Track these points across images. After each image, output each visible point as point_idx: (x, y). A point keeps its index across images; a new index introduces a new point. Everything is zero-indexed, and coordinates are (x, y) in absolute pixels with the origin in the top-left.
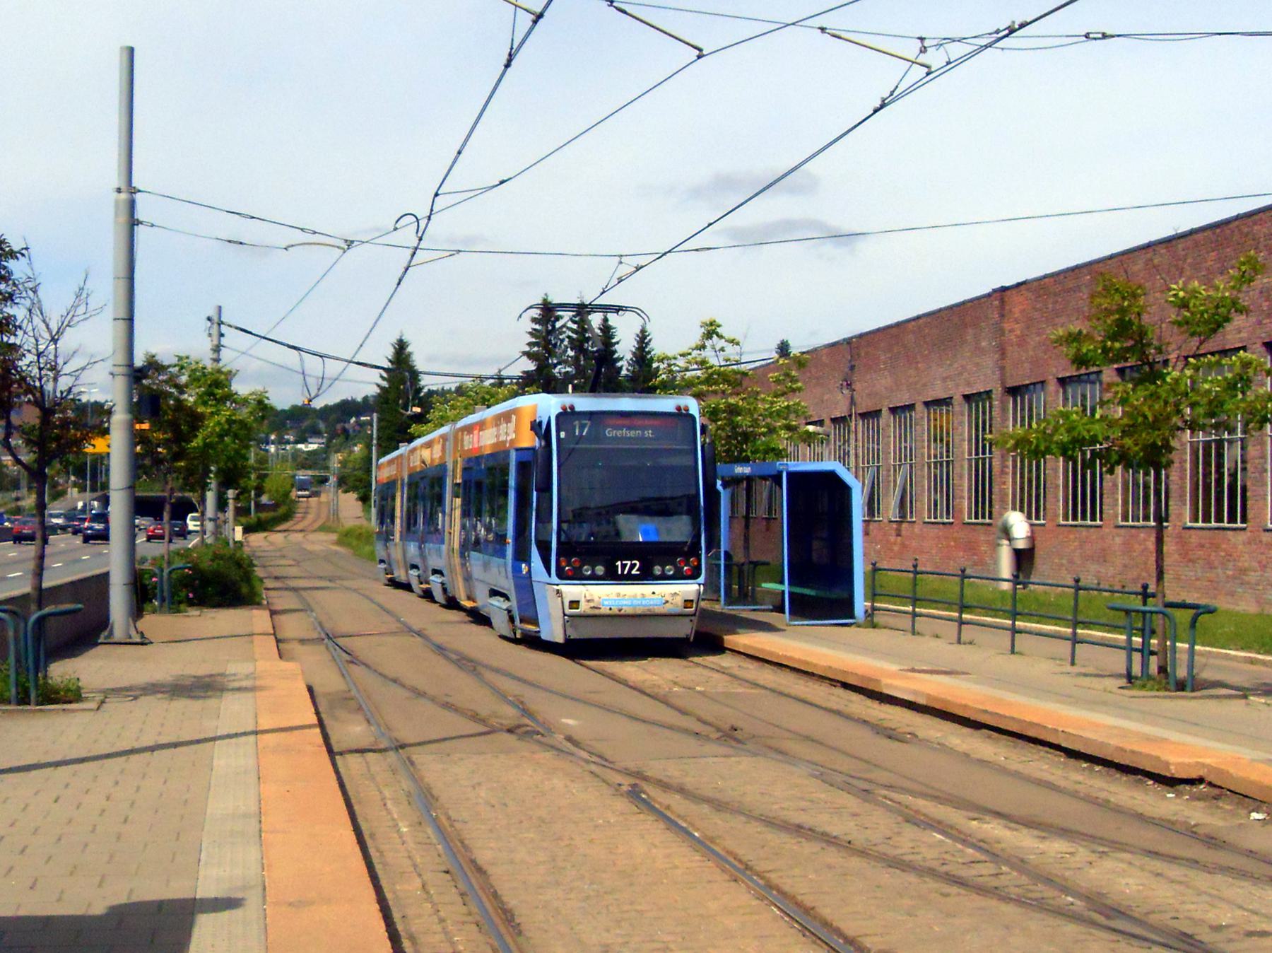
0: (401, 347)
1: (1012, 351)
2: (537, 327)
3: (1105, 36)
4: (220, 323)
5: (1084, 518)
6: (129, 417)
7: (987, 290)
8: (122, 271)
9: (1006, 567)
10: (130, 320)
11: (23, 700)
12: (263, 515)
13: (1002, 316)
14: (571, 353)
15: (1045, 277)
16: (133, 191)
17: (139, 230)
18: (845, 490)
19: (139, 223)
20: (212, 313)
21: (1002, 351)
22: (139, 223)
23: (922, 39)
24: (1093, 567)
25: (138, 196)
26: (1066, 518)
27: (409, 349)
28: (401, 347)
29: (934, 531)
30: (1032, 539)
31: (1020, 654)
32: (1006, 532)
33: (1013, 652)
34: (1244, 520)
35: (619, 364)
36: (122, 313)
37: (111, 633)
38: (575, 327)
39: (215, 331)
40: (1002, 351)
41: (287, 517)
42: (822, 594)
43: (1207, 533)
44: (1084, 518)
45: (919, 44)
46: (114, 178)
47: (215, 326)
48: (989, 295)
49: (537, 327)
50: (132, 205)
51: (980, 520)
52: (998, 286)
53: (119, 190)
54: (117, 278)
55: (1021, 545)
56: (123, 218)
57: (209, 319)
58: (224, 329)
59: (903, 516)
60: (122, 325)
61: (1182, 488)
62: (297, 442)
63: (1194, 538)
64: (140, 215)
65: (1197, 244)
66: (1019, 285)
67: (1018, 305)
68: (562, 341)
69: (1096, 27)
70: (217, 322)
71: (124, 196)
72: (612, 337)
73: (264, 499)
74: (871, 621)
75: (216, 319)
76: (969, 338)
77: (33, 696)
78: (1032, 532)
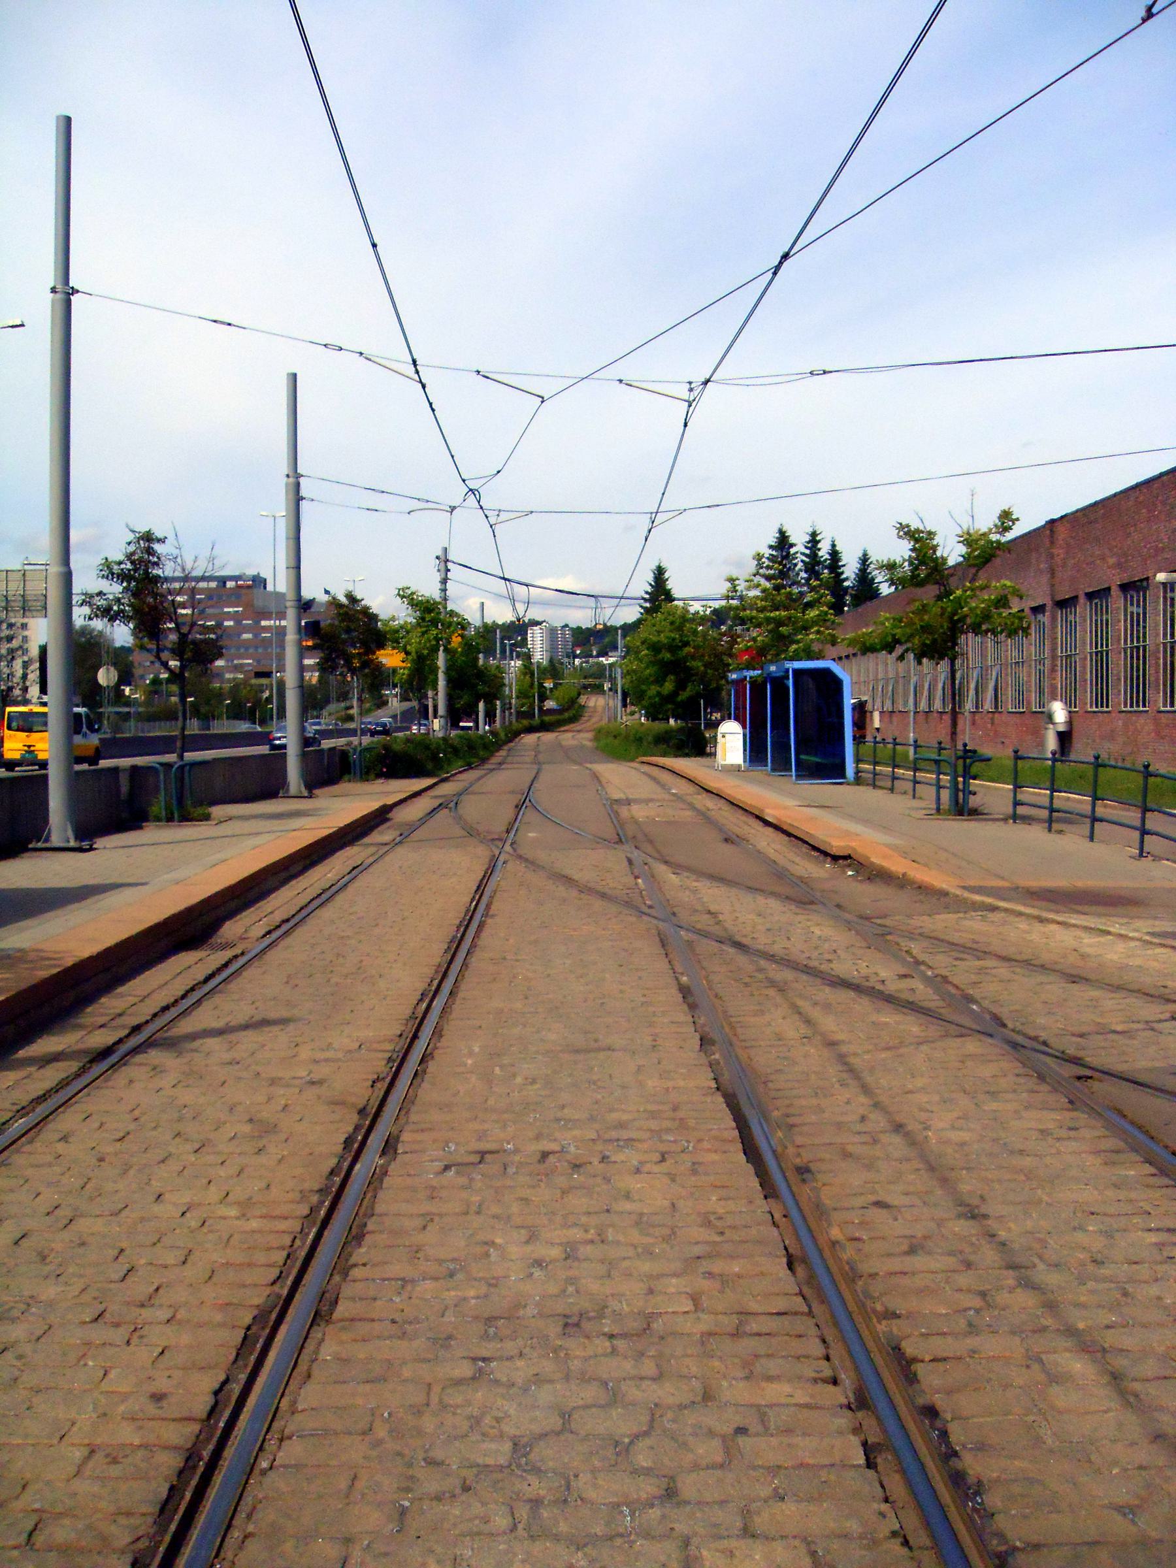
0: (660, 573)
1: (1059, 574)
2: (774, 553)
3: (825, 372)
4: (447, 561)
5: (1138, 706)
6: (298, 637)
7: (1043, 523)
8: (292, 534)
9: (1052, 743)
10: (298, 568)
11: (170, 819)
12: (547, 718)
13: (1052, 543)
14: (803, 575)
15: (1077, 511)
16: (298, 476)
17: (303, 504)
18: (837, 683)
19: (303, 499)
20: (440, 553)
21: (1052, 572)
22: (303, 499)
23: (690, 383)
24: (1107, 745)
25: (302, 480)
26: (1125, 706)
27: (666, 575)
28: (660, 573)
29: (1016, 719)
30: (1070, 723)
31: (920, 798)
32: (1050, 717)
33: (914, 797)
34: (1172, 705)
35: (846, 584)
36: (293, 564)
37: (288, 790)
38: (808, 552)
39: (443, 568)
40: (1052, 572)
41: (574, 719)
42: (824, 761)
43: (1170, 715)
44: (1138, 706)
45: (688, 386)
46: (284, 468)
47: (443, 564)
48: (1043, 527)
49: (774, 553)
50: (298, 485)
51: (1100, 709)
52: (1048, 519)
53: (288, 476)
54: (287, 538)
55: (1061, 728)
56: (292, 496)
57: (437, 558)
58: (450, 565)
59: (996, 707)
60: (292, 572)
61: (1157, 680)
62: (598, 656)
63: (1164, 719)
64: (303, 493)
65: (1163, 485)
66: (1062, 517)
67: (1062, 532)
68: (796, 565)
69: (818, 366)
70: (444, 560)
71: (291, 480)
72: (839, 560)
73: (550, 704)
74: (858, 781)
75: (443, 558)
76: (1034, 561)
77: (176, 815)
78: (1070, 718)
